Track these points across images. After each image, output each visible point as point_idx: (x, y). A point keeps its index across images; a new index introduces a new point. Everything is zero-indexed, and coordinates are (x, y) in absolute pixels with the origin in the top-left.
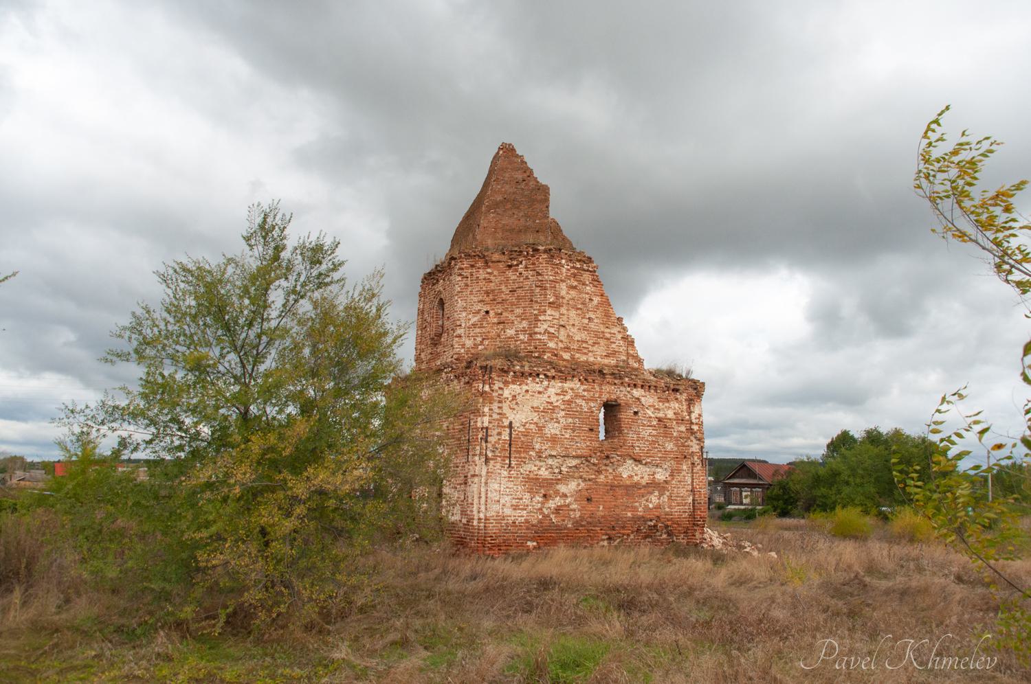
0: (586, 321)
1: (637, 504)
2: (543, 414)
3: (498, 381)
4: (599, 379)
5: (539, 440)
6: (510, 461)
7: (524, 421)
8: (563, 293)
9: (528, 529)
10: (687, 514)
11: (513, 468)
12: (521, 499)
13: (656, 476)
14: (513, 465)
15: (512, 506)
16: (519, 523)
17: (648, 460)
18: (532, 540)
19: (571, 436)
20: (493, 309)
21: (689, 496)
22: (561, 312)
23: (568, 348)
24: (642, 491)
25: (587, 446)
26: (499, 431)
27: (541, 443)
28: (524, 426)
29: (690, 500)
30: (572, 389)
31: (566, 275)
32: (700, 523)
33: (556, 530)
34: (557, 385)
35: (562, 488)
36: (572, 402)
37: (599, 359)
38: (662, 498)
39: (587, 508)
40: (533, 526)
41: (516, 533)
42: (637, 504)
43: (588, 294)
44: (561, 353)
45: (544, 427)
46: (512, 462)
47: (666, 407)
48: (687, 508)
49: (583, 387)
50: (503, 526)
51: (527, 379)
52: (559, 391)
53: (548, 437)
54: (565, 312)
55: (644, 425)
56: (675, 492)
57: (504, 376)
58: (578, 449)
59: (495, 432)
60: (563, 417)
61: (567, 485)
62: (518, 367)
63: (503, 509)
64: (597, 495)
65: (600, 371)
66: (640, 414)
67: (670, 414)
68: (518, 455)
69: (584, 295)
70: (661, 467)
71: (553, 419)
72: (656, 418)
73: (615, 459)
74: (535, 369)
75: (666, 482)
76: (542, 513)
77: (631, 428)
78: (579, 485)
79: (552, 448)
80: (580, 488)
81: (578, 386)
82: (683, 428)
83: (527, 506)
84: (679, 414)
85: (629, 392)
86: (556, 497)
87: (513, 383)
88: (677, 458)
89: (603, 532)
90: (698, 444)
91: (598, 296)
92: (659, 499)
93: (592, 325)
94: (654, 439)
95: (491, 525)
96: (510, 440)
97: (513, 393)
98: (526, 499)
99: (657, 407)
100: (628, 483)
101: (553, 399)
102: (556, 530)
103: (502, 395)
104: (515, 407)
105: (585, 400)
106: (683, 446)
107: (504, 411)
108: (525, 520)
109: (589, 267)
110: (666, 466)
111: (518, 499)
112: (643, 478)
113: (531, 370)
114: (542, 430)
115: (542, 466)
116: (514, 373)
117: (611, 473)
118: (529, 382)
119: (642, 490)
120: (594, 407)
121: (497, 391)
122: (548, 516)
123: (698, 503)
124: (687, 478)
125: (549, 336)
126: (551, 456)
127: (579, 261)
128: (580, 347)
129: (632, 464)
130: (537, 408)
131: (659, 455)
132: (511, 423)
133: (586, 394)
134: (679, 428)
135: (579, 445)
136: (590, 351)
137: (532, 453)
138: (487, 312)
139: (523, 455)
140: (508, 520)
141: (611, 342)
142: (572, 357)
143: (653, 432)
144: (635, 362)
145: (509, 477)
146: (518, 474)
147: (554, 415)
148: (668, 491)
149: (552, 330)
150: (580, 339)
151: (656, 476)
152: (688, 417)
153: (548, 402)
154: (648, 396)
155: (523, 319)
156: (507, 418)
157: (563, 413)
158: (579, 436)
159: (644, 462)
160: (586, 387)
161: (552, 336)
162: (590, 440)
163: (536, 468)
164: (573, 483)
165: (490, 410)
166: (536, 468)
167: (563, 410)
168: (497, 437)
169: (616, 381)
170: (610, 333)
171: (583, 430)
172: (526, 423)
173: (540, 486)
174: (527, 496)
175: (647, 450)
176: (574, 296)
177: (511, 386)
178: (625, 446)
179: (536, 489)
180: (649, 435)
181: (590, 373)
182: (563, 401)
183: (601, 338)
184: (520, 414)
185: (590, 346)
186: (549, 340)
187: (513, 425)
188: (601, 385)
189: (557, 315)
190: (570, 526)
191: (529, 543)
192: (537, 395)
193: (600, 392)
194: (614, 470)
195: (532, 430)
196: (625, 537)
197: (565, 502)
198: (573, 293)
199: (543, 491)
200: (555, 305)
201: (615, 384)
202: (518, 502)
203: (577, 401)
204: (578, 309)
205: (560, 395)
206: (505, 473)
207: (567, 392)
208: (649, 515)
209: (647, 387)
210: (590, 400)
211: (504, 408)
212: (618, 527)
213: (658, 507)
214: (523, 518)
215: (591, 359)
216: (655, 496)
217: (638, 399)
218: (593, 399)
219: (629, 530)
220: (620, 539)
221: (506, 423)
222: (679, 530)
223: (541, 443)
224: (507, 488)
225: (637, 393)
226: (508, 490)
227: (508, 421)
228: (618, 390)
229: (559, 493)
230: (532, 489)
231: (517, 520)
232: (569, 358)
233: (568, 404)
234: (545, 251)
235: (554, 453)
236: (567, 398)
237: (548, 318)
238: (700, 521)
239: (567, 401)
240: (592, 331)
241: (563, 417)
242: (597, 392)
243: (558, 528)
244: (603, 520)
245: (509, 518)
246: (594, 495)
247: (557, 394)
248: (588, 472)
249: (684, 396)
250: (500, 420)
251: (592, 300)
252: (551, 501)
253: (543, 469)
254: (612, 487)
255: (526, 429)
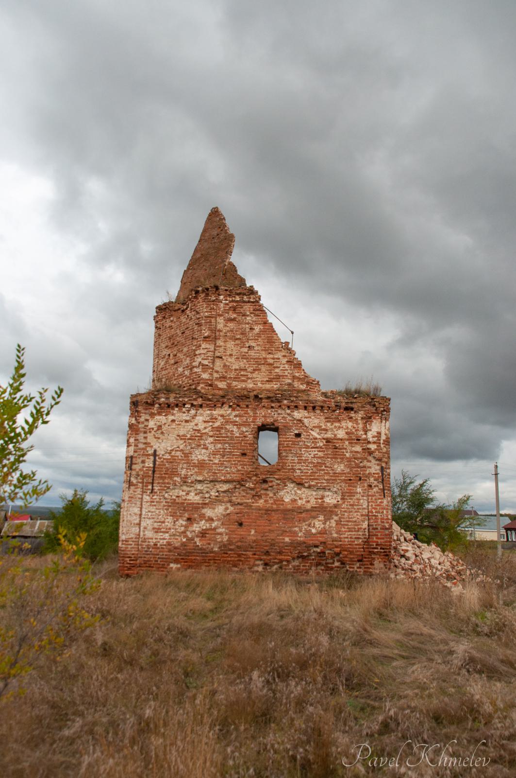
0: (246, 350)
1: (297, 529)
2: (190, 441)
3: (145, 413)
4: (254, 404)
5: (185, 466)
6: (153, 486)
7: (169, 449)
8: (220, 326)
9: (170, 551)
10: (360, 541)
11: (156, 493)
12: (164, 522)
13: (325, 500)
14: (155, 491)
15: (154, 529)
16: (161, 545)
17: (313, 483)
18: (176, 561)
19: (220, 461)
20: (172, 352)
21: (363, 521)
22: (218, 344)
23: (224, 378)
24: (303, 515)
25: (239, 471)
26: (144, 459)
27: (187, 469)
28: (170, 453)
29: (365, 525)
30: (222, 416)
31: (224, 310)
32: (376, 550)
33: (202, 553)
34: (206, 413)
35: (208, 512)
36: (222, 428)
37: (259, 385)
38: (328, 523)
39: (236, 533)
40: (175, 548)
41: (158, 555)
42: (297, 529)
43: (248, 323)
44: (216, 383)
45: (191, 454)
46: (155, 488)
47: (335, 427)
48: (361, 533)
49: (234, 413)
50: (145, 548)
51: (174, 409)
52: (208, 419)
53: (195, 463)
54: (222, 344)
55: (307, 447)
56: (346, 516)
57: (150, 409)
58: (227, 473)
59: (139, 461)
60: (212, 443)
61: (214, 509)
62: (163, 400)
63: (144, 531)
64: (248, 519)
65: (256, 397)
66: (302, 436)
67: (341, 434)
68: (161, 481)
69: (244, 326)
70: (329, 489)
71: (200, 446)
72: (324, 439)
73: (274, 484)
74: (181, 399)
75: (336, 506)
76: (186, 536)
77: (291, 450)
78: (227, 509)
79: (199, 473)
80: (228, 512)
81: (228, 412)
82: (358, 448)
83: (170, 529)
84: (353, 433)
85: (289, 414)
86: (201, 520)
87: (159, 414)
88: (350, 480)
89: (256, 556)
90: (378, 465)
91: (259, 324)
92: (324, 523)
93: (252, 353)
94: (320, 461)
95: (129, 546)
96: (154, 467)
97: (158, 424)
98: (168, 522)
99: (323, 427)
100: (290, 507)
101: (201, 426)
102: (202, 553)
103: (147, 426)
104: (160, 436)
105: (237, 425)
106: (358, 468)
107: (149, 441)
108: (167, 542)
109: (250, 298)
110: (335, 489)
111: (159, 522)
112: (308, 502)
113: (177, 401)
114: (188, 457)
115: (190, 491)
116: (160, 405)
117: (272, 497)
118: (175, 412)
119: (304, 514)
120: (247, 432)
121: (143, 423)
122: (192, 539)
123: (374, 529)
124: (362, 501)
125: (202, 369)
126: (200, 482)
127: (238, 294)
128: (238, 375)
129: (294, 487)
130: (183, 436)
131: (326, 478)
132: (155, 451)
133: (237, 419)
134: (353, 449)
135: (229, 469)
136: (249, 378)
137: (177, 479)
138: (169, 355)
139: (166, 481)
140: (149, 542)
141: (275, 367)
142: (229, 385)
143: (320, 453)
144: (302, 384)
145: (152, 502)
146: (160, 499)
147: (202, 442)
148: (337, 515)
149: (206, 362)
150: (237, 367)
151: (325, 500)
152: (364, 436)
153: (196, 430)
154: (312, 417)
155: (187, 357)
156: (152, 447)
157: (211, 439)
158: (229, 461)
159: (306, 485)
160: (238, 412)
161: (205, 368)
162: (241, 465)
163: (184, 493)
164: (220, 507)
165: (135, 440)
166: (184, 493)
167: (211, 436)
168: (141, 465)
169: (273, 405)
170: (273, 359)
171: (234, 455)
172: (172, 450)
173: (184, 510)
174: (170, 519)
175: (311, 473)
176: (232, 327)
177: (157, 417)
178: (284, 469)
179: (180, 513)
180: (314, 457)
181: (242, 399)
182: (213, 428)
183: (263, 364)
184: (166, 442)
185: (249, 374)
186: (202, 371)
187: (157, 453)
188: (254, 410)
189: (212, 347)
190: (216, 549)
191: (172, 565)
192: (183, 424)
193: (254, 416)
194: (275, 494)
195: (178, 456)
196: (285, 563)
197: (211, 526)
198: (231, 325)
199: (186, 515)
200: (212, 338)
201: (272, 407)
202: (160, 526)
203: (228, 427)
204: (237, 339)
205: (209, 422)
206: (148, 498)
207: (216, 419)
208: (312, 540)
209: (311, 408)
210: (242, 425)
211: (149, 437)
212: (274, 552)
213: (323, 532)
214: (165, 541)
215: (250, 385)
216: (319, 521)
217: (300, 420)
218: (246, 424)
219: (289, 556)
220: (279, 565)
221: (151, 451)
222: (351, 558)
223: (187, 469)
224: (149, 511)
225: (297, 414)
226: (150, 514)
227: (153, 450)
228: (275, 413)
229: (205, 517)
230: (176, 513)
231: (159, 542)
232: (225, 387)
233: (217, 431)
234: (203, 291)
235: (200, 478)
236: (217, 424)
237: (202, 351)
238: (377, 548)
239: (216, 427)
240: (251, 358)
241: (212, 443)
242: (251, 416)
243: (203, 551)
244: (254, 544)
245: (150, 540)
246: (245, 519)
247: (205, 422)
248: (244, 496)
249: (361, 414)
250: (144, 449)
251: (254, 329)
252: (195, 525)
253: (192, 494)
254: (268, 511)
255: (172, 456)
